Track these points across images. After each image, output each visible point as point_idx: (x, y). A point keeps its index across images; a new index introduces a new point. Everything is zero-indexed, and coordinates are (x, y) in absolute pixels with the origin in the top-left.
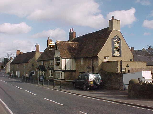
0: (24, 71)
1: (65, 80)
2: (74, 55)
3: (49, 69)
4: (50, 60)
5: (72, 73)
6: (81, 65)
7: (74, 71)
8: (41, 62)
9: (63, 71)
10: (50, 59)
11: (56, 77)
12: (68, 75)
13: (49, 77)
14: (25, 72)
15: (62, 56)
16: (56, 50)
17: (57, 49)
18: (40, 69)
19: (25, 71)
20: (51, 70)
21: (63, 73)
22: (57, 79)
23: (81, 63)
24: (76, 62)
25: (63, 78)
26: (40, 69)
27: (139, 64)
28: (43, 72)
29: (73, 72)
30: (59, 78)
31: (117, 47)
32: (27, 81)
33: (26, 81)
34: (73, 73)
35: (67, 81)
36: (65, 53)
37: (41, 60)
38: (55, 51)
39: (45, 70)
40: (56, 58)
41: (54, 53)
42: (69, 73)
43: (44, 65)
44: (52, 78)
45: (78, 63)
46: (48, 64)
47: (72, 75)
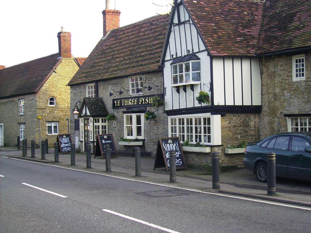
0: (20, 124)
1: (223, 150)
2: (253, 46)
3: (125, 110)
4: (127, 76)
5: (247, 119)
6: (291, 84)
7: (255, 110)
8: (87, 88)
9: (223, 111)
10: (120, 74)
11: (130, 133)
12: (234, 126)
13: (131, 140)
14: (23, 126)
15: (213, 50)
16: (177, 28)
17: (180, 23)
18: (88, 114)
19: (24, 123)
20: (134, 116)
21: (216, 120)
22: (198, 145)
23: (294, 73)
24: (261, 74)
25: (217, 138)
26: (86, 111)
27: (108, 103)
28: (100, 124)
29: (252, 117)
30: (194, 143)
31: (224, 50)
32: (50, 157)
33: (43, 158)
34: (253, 120)
35: (231, 151)
36: (219, 37)
37: (89, 79)
38: (170, 31)
39: (105, 116)
40: (177, 58)
41: (168, 42)
42: (236, 119)
43: (100, 95)
44: (140, 143)
45: (272, 76)
46: (121, 93)
47: (248, 126)
